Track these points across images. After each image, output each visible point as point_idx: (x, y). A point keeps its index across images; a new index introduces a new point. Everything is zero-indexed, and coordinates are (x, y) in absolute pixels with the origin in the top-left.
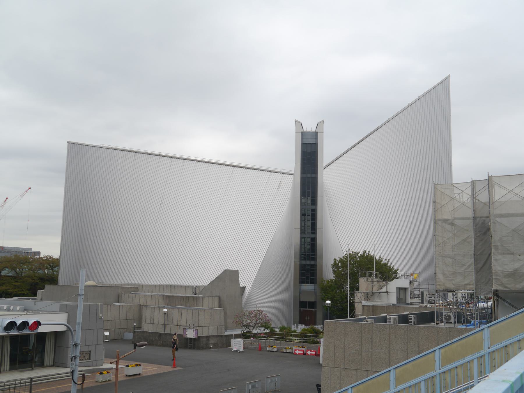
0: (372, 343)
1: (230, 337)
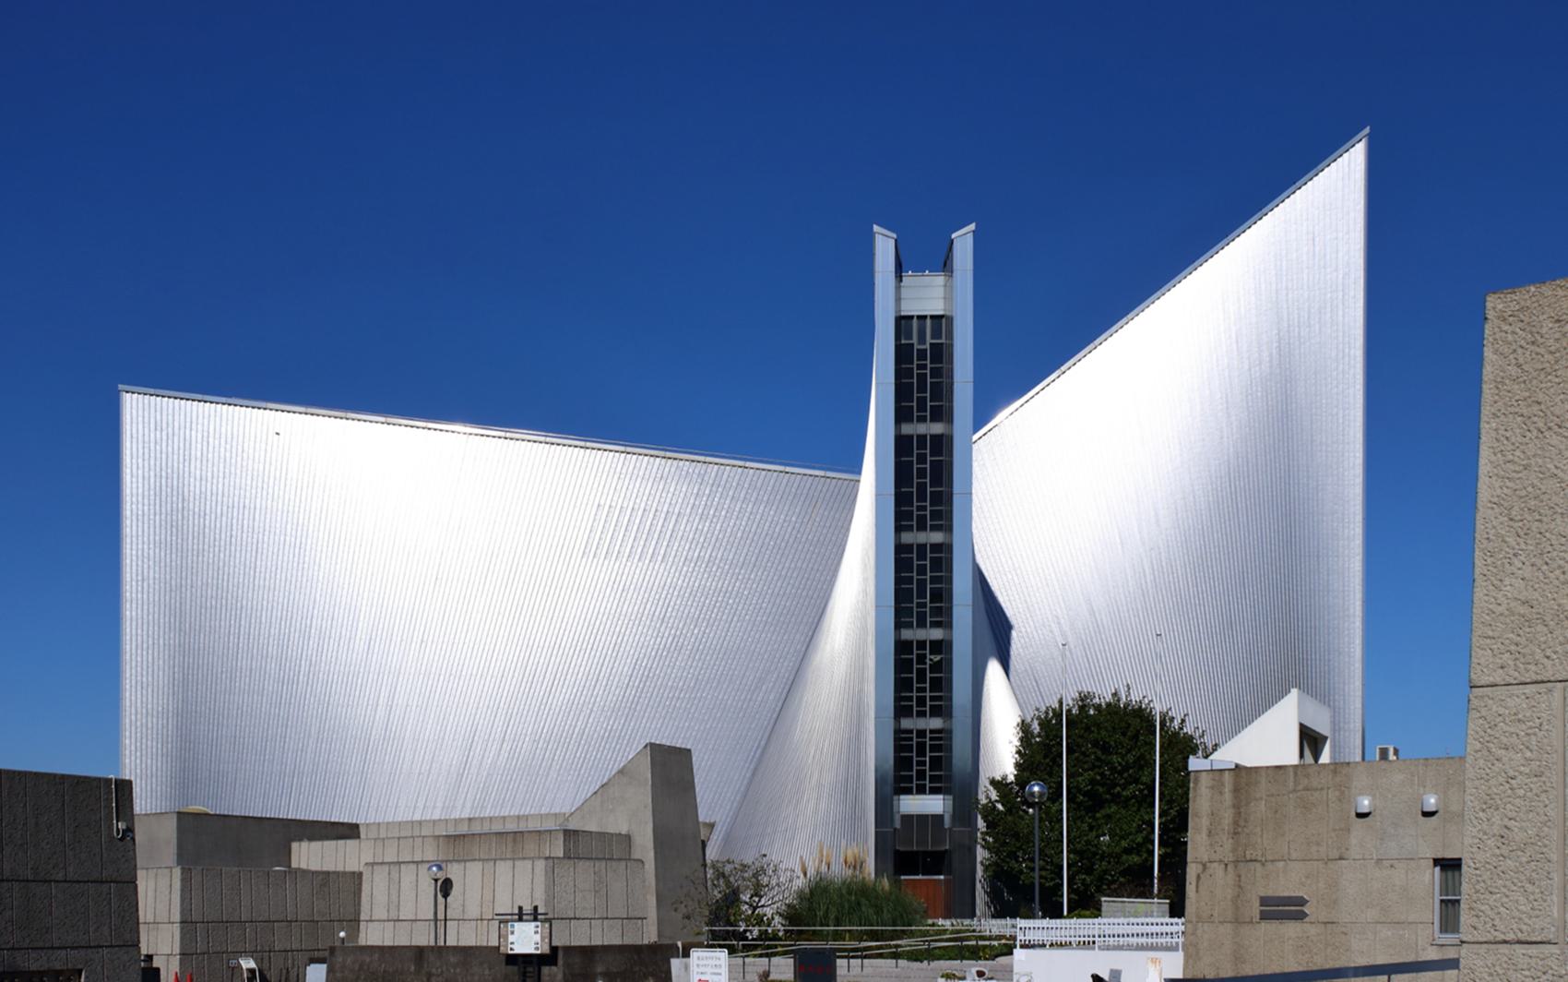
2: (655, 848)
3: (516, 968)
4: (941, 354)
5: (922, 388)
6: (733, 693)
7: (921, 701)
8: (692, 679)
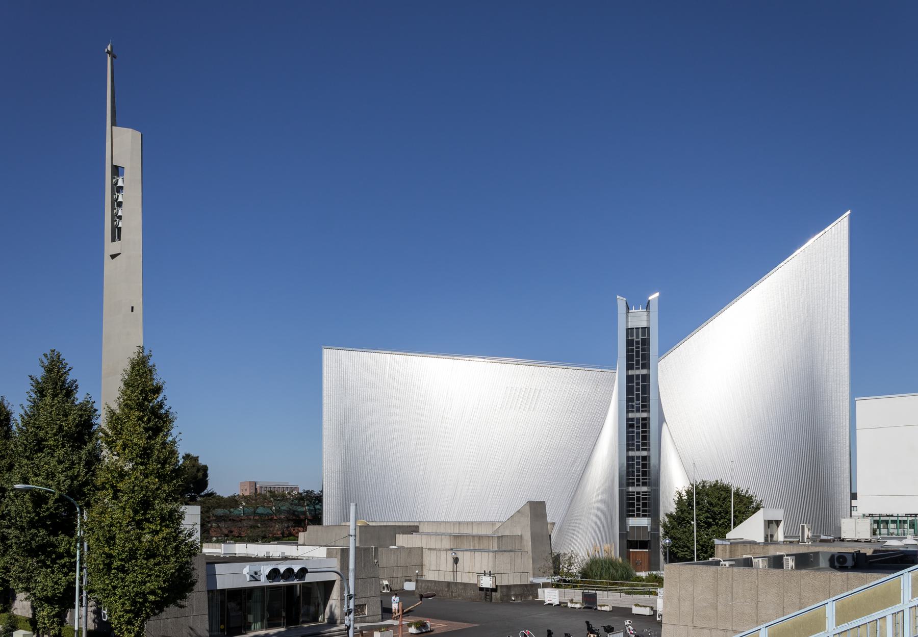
1: (537, 586)
3: (483, 592)
4: (646, 342)
5: (638, 356)
6: (563, 467)
7: (638, 480)
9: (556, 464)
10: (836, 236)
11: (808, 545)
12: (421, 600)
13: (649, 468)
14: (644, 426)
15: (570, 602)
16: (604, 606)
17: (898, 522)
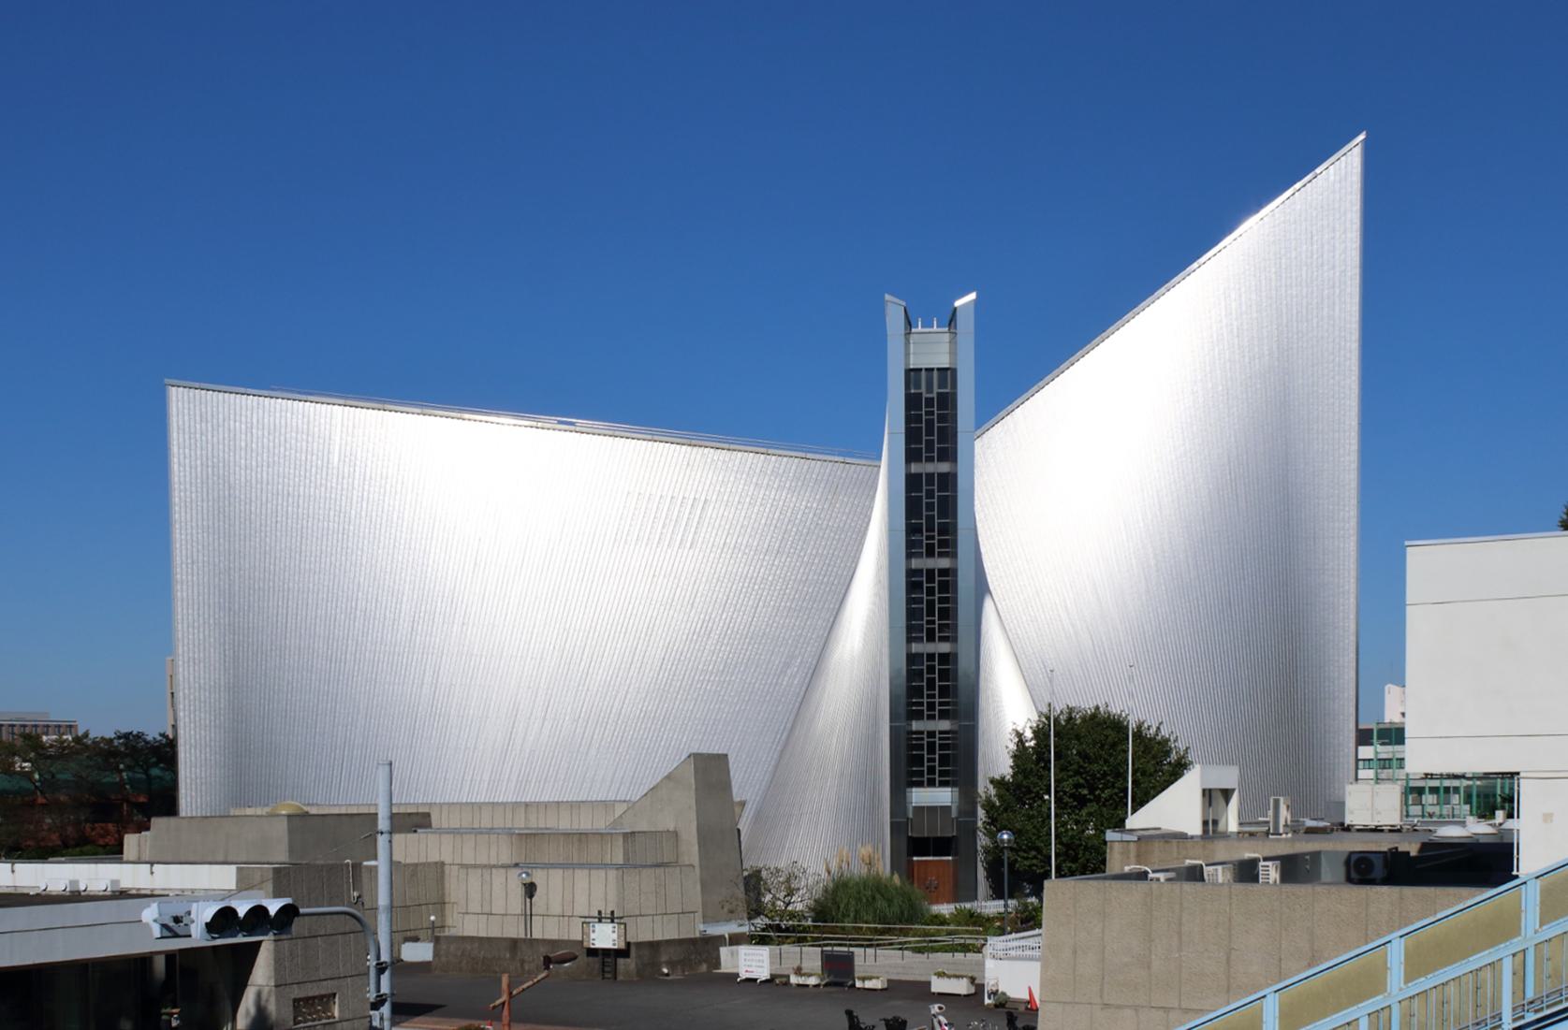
0: (1180, 938)
1: (718, 941)
2: (699, 843)
3: (596, 959)
4: (947, 402)
5: (930, 432)
7: (931, 706)
8: (721, 662)
9: (745, 670)
10: (1337, 186)
11: (1286, 840)
12: (547, 968)
13: (956, 679)
14: (945, 587)
15: (796, 973)
16: (870, 978)
17: (1442, 791)
